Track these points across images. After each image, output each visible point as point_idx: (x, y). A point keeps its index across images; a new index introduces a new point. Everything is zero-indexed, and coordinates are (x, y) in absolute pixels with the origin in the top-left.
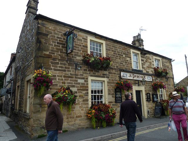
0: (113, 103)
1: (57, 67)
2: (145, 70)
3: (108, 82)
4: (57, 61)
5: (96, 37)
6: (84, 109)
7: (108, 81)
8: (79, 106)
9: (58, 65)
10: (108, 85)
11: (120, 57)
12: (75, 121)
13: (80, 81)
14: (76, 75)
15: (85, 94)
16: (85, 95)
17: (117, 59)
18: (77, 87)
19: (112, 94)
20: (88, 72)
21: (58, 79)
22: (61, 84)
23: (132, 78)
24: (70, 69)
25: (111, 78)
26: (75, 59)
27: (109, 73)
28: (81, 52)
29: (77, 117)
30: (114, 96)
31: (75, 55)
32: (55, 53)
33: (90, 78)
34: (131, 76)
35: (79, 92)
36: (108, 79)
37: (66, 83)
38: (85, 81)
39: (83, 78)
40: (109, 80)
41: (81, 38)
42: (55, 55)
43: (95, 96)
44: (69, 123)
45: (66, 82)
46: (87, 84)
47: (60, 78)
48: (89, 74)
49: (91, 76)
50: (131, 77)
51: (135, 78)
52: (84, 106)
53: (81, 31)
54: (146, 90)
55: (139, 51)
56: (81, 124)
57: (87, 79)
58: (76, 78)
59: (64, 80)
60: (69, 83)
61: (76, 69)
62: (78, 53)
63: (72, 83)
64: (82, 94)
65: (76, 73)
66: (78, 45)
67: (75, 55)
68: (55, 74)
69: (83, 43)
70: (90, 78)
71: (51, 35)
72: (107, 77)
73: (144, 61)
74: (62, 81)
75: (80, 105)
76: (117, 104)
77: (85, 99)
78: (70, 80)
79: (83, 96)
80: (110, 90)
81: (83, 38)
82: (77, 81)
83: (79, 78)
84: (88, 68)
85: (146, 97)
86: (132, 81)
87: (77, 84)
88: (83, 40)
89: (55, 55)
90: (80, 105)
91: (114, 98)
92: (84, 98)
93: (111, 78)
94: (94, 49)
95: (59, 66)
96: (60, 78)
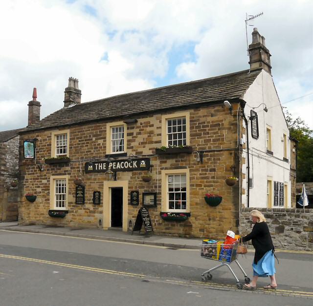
2: (134, 151)
3: (69, 180)
20: (51, 172)
29: (41, 214)
33: (52, 177)
39: (46, 179)
40: (71, 176)
49: (53, 175)
54: (130, 186)
57: (49, 178)
58: (41, 179)
82: (41, 182)
85: (130, 198)
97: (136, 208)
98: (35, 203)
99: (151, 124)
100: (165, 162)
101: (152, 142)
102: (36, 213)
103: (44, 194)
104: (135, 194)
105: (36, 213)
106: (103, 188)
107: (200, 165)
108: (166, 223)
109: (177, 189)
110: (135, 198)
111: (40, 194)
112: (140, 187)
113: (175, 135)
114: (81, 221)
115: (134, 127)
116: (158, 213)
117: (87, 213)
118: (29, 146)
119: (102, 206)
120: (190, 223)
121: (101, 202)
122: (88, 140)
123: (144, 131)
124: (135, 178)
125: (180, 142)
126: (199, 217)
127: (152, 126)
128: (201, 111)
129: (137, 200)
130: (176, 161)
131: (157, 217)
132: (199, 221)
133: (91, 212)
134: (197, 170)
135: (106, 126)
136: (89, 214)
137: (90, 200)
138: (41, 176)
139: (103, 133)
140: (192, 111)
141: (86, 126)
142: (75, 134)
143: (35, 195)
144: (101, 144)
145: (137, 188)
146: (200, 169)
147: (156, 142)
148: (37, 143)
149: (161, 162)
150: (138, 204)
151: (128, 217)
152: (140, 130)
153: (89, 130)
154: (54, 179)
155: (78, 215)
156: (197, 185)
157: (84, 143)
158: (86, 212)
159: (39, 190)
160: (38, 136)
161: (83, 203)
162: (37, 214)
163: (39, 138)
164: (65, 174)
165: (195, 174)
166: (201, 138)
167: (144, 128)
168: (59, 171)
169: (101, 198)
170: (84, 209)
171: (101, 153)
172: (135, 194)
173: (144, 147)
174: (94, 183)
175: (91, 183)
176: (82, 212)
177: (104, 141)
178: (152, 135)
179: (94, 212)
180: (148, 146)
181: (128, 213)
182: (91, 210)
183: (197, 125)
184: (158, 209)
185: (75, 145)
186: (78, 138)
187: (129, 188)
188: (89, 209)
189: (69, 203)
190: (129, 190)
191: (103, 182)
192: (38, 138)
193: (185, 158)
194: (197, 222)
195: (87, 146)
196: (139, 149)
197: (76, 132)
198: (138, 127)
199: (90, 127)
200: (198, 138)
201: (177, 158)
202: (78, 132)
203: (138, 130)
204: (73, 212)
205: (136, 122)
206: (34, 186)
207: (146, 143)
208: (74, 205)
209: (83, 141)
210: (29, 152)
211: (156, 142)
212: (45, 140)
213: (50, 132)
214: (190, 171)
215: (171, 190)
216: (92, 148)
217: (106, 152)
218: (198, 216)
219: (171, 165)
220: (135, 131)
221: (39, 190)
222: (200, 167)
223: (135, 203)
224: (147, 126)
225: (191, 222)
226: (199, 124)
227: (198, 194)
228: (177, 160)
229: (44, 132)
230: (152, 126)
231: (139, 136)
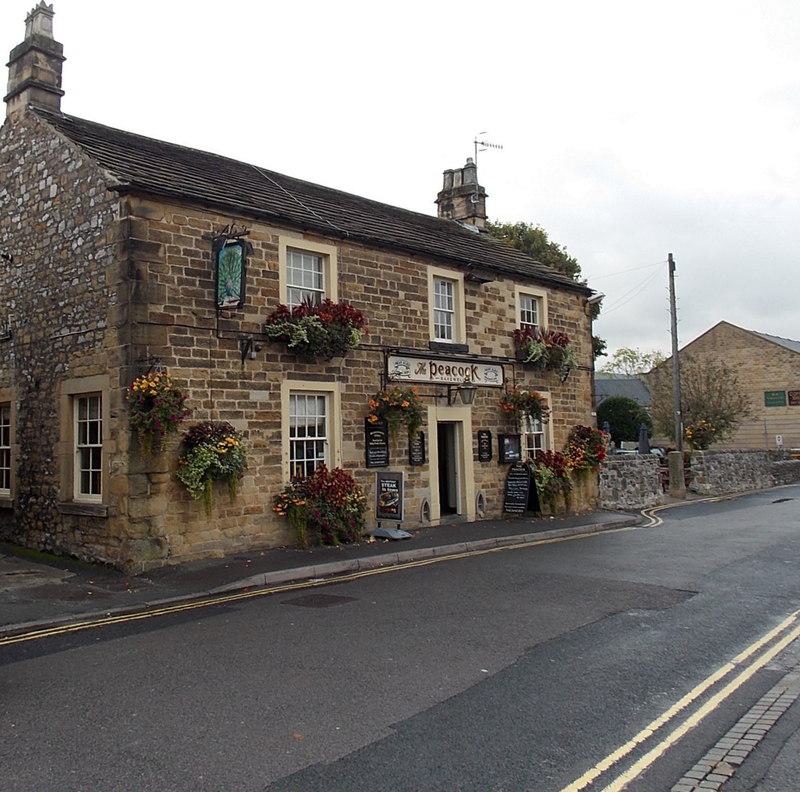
0: (357, 466)
3: (344, 397)
5: (306, 236)
14: (244, 376)
15: (272, 437)
16: (271, 442)
18: (247, 417)
20: (281, 365)
21: (194, 393)
23: (426, 377)
27: (348, 363)
28: (259, 295)
29: (247, 512)
30: (363, 443)
33: (287, 386)
34: (422, 370)
37: (216, 405)
39: (267, 387)
44: (226, 530)
45: (215, 400)
46: (279, 405)
47: (199, 390)
49: (290, 377)
57: (278, 387)
60: (225, 405)
63: (234, 403)
65: (245, 370)
72: (340, 378)
73: (478, 310)
78: (228, 396)
80: (350, 423)
82: (247, 396)
83: (254, 387)
85: (477, 447)
87: (246, 406)
92: (268, 451)
96: (199, 390)
141: (399, 259)
157: (379, 300)
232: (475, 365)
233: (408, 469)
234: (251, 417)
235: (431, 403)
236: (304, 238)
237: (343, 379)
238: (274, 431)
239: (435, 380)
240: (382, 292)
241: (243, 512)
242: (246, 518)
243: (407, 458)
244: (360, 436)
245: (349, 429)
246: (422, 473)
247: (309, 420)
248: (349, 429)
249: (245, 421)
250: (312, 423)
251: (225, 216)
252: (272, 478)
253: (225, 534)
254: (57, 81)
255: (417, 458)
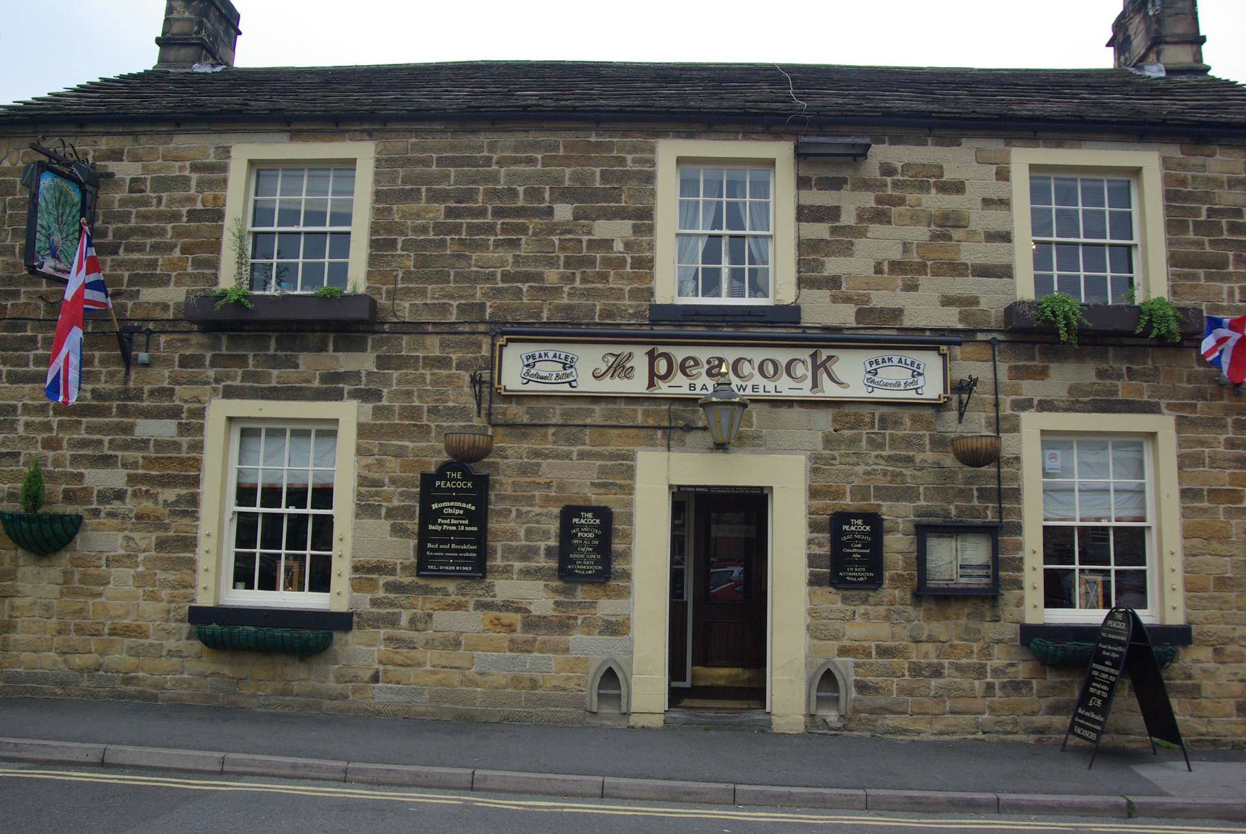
0: (392, 571)
1: (27, 365)
2: (848, 300)
3: (364, 431)
4: (29, 333)
5: (296, 135)
6: (165, 593)
7: (368, 418)
8: (132, 572)
9: (31, 354)
10: (360, 451)
11: (506, 229)
12: (102, 654)
13: (147, 428)
14: (126, 394)
15: (177, 502)
16: (173, 513)
17: (482, 246)
18: (125, 466)
19: (391, 513)
20: (211, 373)
21: (28, 425)
22: (38, 450)
23: (637, 384)
24: (97, 367)
25: (395, 395)
26: (130, 304)
27: (383, 362)
28: (177, 253)
29: (114, 632)
30: (413, 525)
31: (133, 280)
32: (23, 290)
33: (219, 410)
34: (620, 368)
35: (135, 494)
36: (369, 407)
37: (65, 444)
38: (184, 429)
39: (174, 413)
40: (378, 411)
41: (182, 168)
42: (23, 300)
43: (273, 521)
44: (68, 656)
45: (65, 437)
46: (198, 447)
47: (37, 419)
48: (217, 381)
49: (229, 393)
50: (628, 373)
51: (679, 378)
52: (161, 575)
53: (81, 126)
54: (821, 482)
55: (778, 136)
56: (141, 674)
57: (200, 413)
58: (123, 411)
59: (55, 426)
60: (84, 444)
61: (128, 361)
62: (153, 264)
63: (100, 442)
64: (157, 503)
65: (131, 385)
66: (160, 216)
67: (133, 280)
68: (13, 398)
69: (191, 200)
70: (219, 410)
71: (8, 198)
72: (356, 394)
74: (46, 435)
75: (141, 569)
76: (435, 584)
77: (172, 534)
78: (90, 429)
79: (158, 518)
80: (376, 483)
81: (195, 168)
82: (129, 429)
83: (147, 414)
84: (215, 346)
85: (825, 550)
86: (640, 409)
87: (126, 446)
88: (195, 177)
89: (23, 300)
90: (141, 569)
91: (413, 542)
92: (166, 528)
93: (395, 395)
94: (1068, 222)
95: (36, 357)
96: (37, 419)
97: (865, 601)
98: (64, 559)
99: (948, 176)
100: (1042, 374)
101: (956, 269)
102: (72, 622)
103: (147, 505)
104: (858, 525)
105: (72, 622)
106: (629, 490)
107: (1226, 402)
108: (1052, 678)
109: (272, 495)
110: (856, 551)
111: (116, 505)
112: (885, 493)
113: (1093, 251)
114: (455, 677)
115: (845, 181)
116: (1010, 631)
117: (510, 628)
118: (61, 200)
119: (624, 593)
120: (1190, 677)
121: (617, 566)
122: (520, 212)
123: (902, 209)
124: (854, 441)
125: (313, 274)
126: (1230, 648)
127: (958, 187)
128: (1218, 157)
129: (874, 561)
130: (1101, 374)
131: (996, 649)
132: (1232, 667)
133: (532, 623)
134: (1215, 424)
135: (652, 150)
136: (519, 635)
137: (527, 554)
138: (126, 394)
139: (634, 184)
140: (1174, 152)
141: (561, 139)
142: (419, 169)
143: (70, 509)
144: (619, 246)
145: (866, 497)
146: (1229, 420)
147: (984, 271)
148: (102, 197)
149: (1019, 373)
150: (875, 582)
151: (811, 653)
152: (879, 201)
153: (531, 161)
154: (231, 420)
155: (429, 644)
156: (1215, 495)
157: (490, 229)
158: (497, 623)
159: (99, 479)
160: (117, 156)
161: (479, 568)
162: (80, 630)
163: (125, 170)
164: (337, 396)
165: (1202, 443)
166: (1226, 278)
167: (911, 197)
168: (276, 376)
169: (617, 546)
170: (481, 606)
171: (619, 294)
172: (858, 525)
173: (911, 287)
174: (568, 456)
175: (537, 454)
176: (469, 622)
177: (637, 230)
178: (957, 234)
179: (564, 626)
180: (932, 287)
181: (808, 627)
182: (536, 610)
183: (1203, 217)
184: (1008, 611)
185: (416, 230)
186: (435, 197)
187: (814, 493)
188: (518, 610)
189: (356, 569)
190: (819, 503)
191: (630, 457)
192: (112, 166)
193: (1150, 364)
194: (1224, 671)
195: (514, 244)
196: (873, 294)
197: (426, 163)
198: (866, 185)
199: (535, 146)
200: (1209, 277)
201: (1104, 357)
202: (441, 161)
203: (868, 200)
204: (393, 621)
205: (860, 154)
206: (67, 453)
207: (921, 269)
208: (407, 580)
209: (482, 212)
210: (57, 237)
211: (984, 271)
212: (163, 184)
213: (224, 140)
214: (1181, 424)
215: (245, 494)
216: (552, 263)
217: (651, 292)
218: (1232, 640)
219: (1070, 391)
220: (851, 203)
221: (99, 479)
222: (1228, 411)
223: (858, 573)
224: (923, 187)
225: (1196, 669)
226: (1211, 212)
227: (1225, 539)
228: (1105, 366)
229: (170, 134)
230: (958, 187)
231: (875, 229)
232: (825, 354)
233: (555, 591)
234: (135, 465)
235: (651, 443)
236: (291, 139)
237: (364, 395)
238: (183, 491)
239: (663, 389)
240: (498, 213)
241: (106, 631)
242: (112, 641)
243: (553, 564)
244: (406, 512)
245: (377, 494)
246: (439, 617)
247: (315, 476)
248: (377, 494)
249: (122, 473)
250: (298, 483)
251: (115, 134)
252: (171, 576)
253: (66, 661)
254: (1147, 410)
255: (586, 562)
